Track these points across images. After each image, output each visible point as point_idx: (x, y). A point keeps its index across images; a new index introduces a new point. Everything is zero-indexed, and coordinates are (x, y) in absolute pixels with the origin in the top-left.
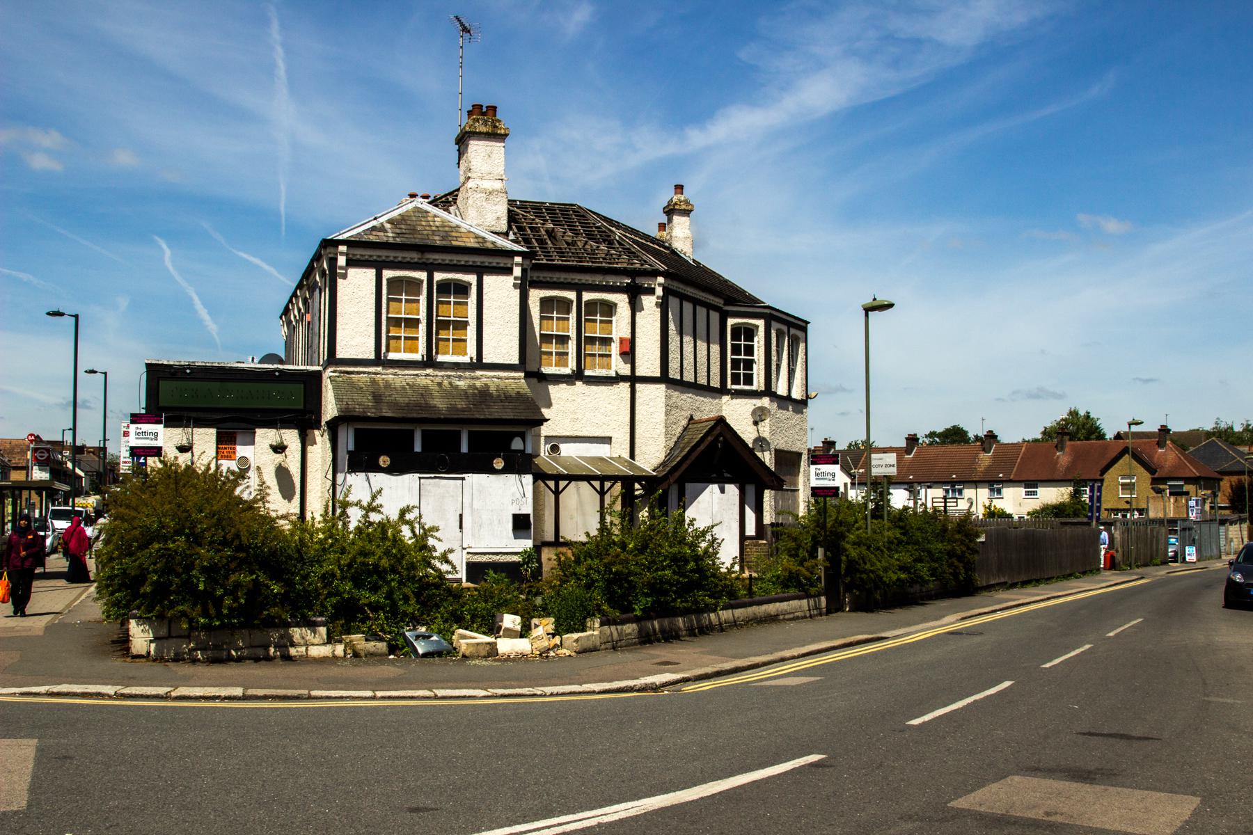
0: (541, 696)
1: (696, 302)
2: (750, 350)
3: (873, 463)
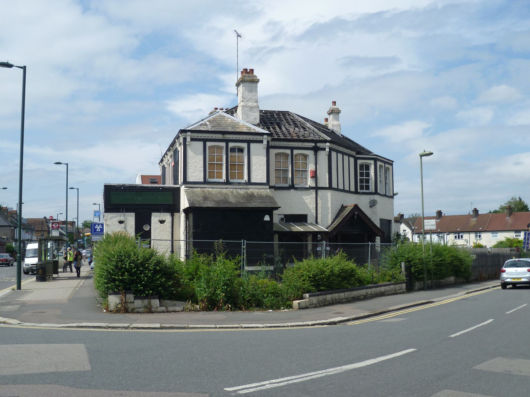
0: (287, 327)
1: (343, 154)
2: (368, 175)
3: (425, 224)
